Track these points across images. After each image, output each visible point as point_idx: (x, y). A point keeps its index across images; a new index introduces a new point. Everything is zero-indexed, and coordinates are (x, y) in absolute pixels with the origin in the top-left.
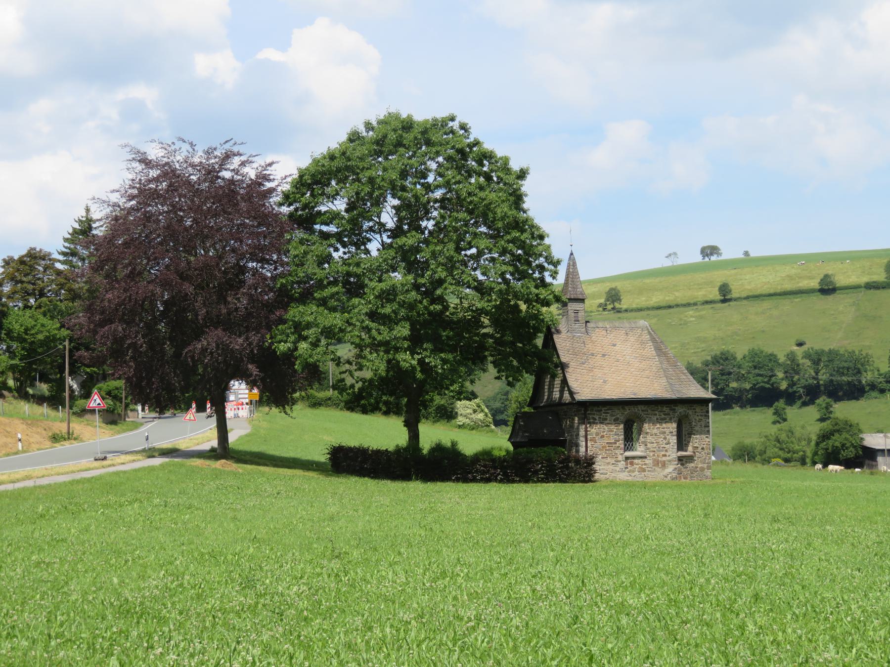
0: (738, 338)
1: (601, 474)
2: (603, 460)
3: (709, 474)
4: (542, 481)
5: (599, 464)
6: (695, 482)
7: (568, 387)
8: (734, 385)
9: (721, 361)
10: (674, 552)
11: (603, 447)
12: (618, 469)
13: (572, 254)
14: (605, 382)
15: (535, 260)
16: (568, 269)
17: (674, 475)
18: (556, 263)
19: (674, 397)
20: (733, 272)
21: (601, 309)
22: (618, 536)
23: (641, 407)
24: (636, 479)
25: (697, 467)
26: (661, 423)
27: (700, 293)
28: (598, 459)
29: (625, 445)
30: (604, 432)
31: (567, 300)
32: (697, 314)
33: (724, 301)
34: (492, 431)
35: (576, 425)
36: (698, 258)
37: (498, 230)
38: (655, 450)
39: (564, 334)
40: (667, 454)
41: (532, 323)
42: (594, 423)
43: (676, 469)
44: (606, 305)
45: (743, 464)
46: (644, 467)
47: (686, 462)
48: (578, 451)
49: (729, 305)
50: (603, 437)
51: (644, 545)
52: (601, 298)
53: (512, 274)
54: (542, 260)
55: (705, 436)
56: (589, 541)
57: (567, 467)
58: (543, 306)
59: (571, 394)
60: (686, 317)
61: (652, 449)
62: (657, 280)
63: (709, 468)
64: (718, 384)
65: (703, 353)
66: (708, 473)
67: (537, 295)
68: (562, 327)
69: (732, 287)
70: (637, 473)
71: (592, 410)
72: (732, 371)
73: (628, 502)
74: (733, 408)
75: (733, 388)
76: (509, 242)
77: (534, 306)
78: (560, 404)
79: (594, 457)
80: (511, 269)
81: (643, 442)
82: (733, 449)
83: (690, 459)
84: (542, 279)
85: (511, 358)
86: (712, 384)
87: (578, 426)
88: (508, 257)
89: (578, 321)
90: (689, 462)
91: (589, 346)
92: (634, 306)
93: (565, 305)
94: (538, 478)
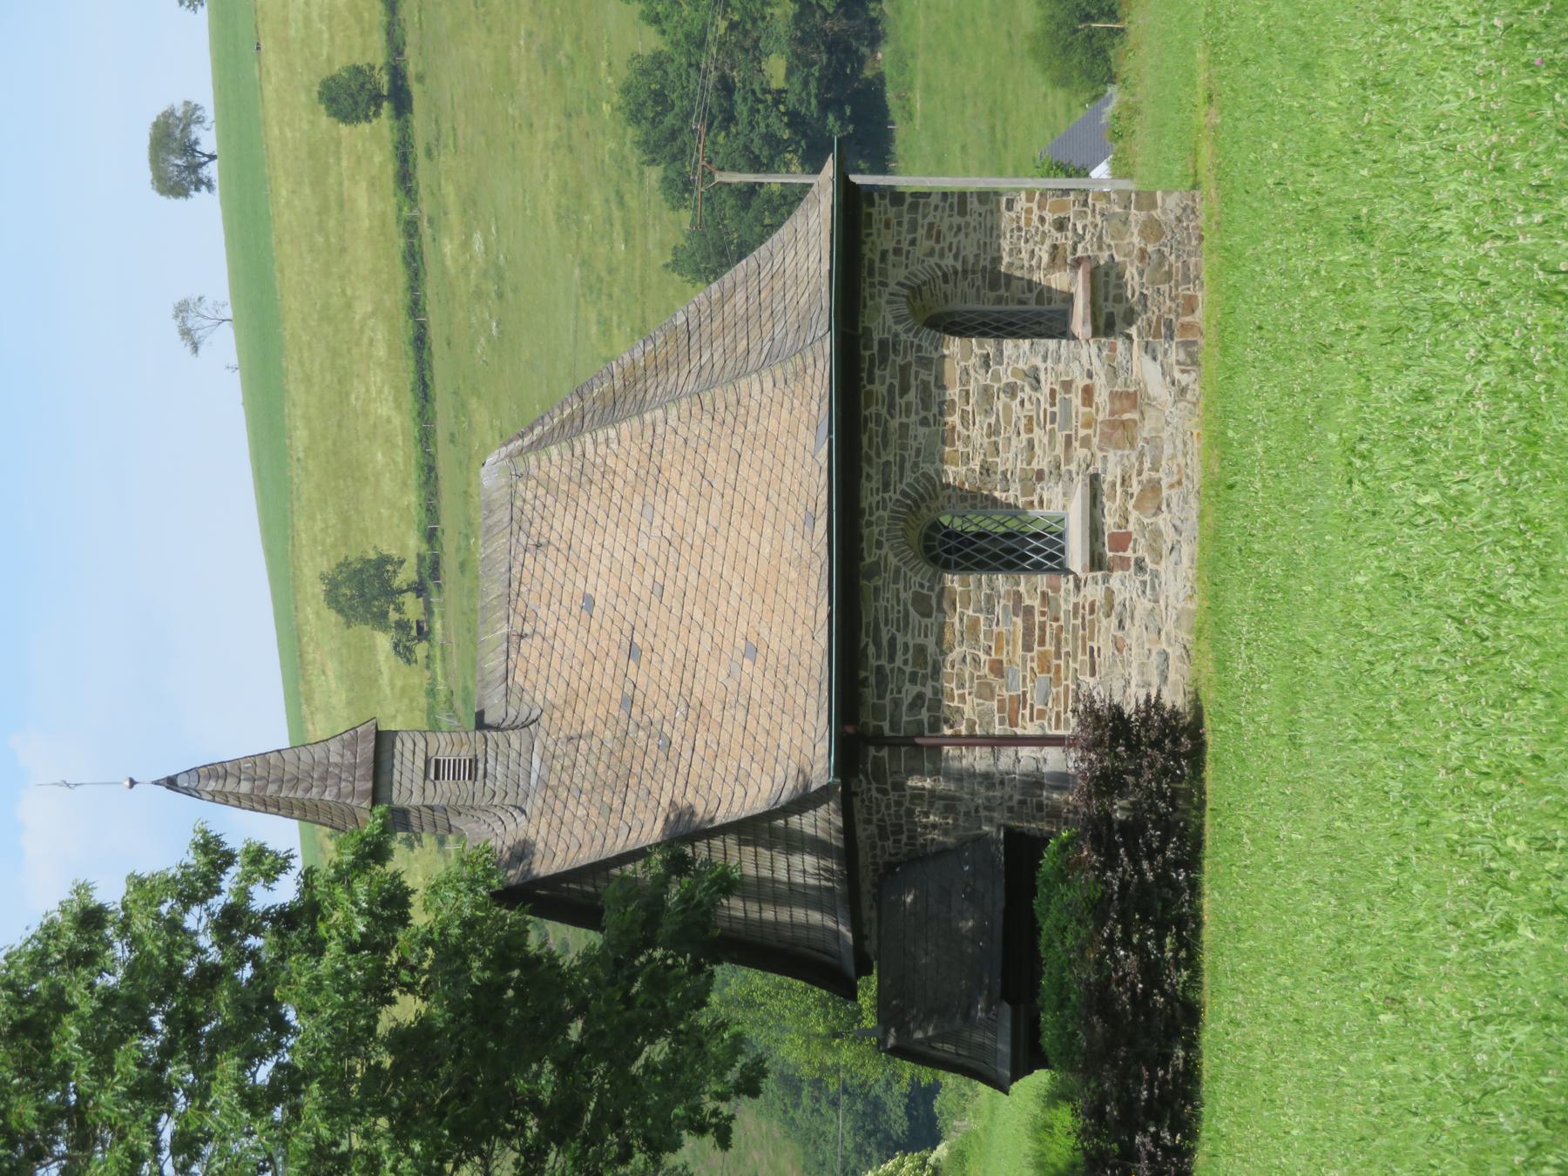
0: (567, 46)
1: (1164, 678)
2: (1101, 670)
3: (1172, 202)
4: (1190, 946)
5: (1117, 685)
6: (1206, 264)
7: (769, 815)
8: (776, 69)
9: (669, 120)
10: (1522, 387)
11: (1045, 667)
12: (1143, 605)
13: (171, 783)
14: (751, 651)
15: (197, 950)
16: (239, 801)
17: (1175, 354)
18: (215, 854)
19: (826, 346)
20: (271, 57)
21: (421, 650)
22: (1450, 627)
23: (869, 495)
24: (1191, 527)
25: (1143, 254)
26: (944, 408)
27: (362, 204)
28: (1100, 694)
29: (1038, 567)
30: (976, 660)
31: (381, 809)
32: (454, 217)
33: (401, 100)
34: (960, 1156)
35: (942, 785)
36: (205, 208)
37: (49, 1118)
38: (1060, 437)
39: (535, 829)
40: (1081, 382)
41: (477, 971)
42: (936, 704)
43: (1147, 347)
44: (402, 626)
45: (1132, 39)
46: (1135, 488)
47: (1119, 298)
48: (1062, 781)
49: (420, 78)
50: (998, 668)
51: (1489, 517)
52: (372, 648)
53: (253, 1055)
54: (194, 919)
55: (1007, 215)
56: (1469, 760)
57: (1131, 830)
58: (404, 920)
59: (804, 801)
60: (465, 271)
61: (1059, 449)
62: (296, 391)
63: (1146, 200)
64: (770, 139)
65: (632, 203)
66: (1168, 205)
67: (352, 948)
68: (501, 834)
69: (340, 64)
70: (1163, 521)
71: (878, 711)
72: (713, 76)
73: (1292, 567)
74: (880, 78)
75: (790, 72)
76: (104, 1069)
77: (402, 962)
78: (848, 852)
79: (1091, 711)
80: (228, 1065)
81: (1028, 490)
82: (1062, 81)
83: (1104, 281)
84: (286, 919)
85: (636, 1068)
86: (769, 168)
87: (948, 776)
88: (179, 1072)
89: (474, 762)
90: (1121, 286)
91: (589, 714)
92: (412, 498)
93: (399, 819)
94: (1178, 964)
